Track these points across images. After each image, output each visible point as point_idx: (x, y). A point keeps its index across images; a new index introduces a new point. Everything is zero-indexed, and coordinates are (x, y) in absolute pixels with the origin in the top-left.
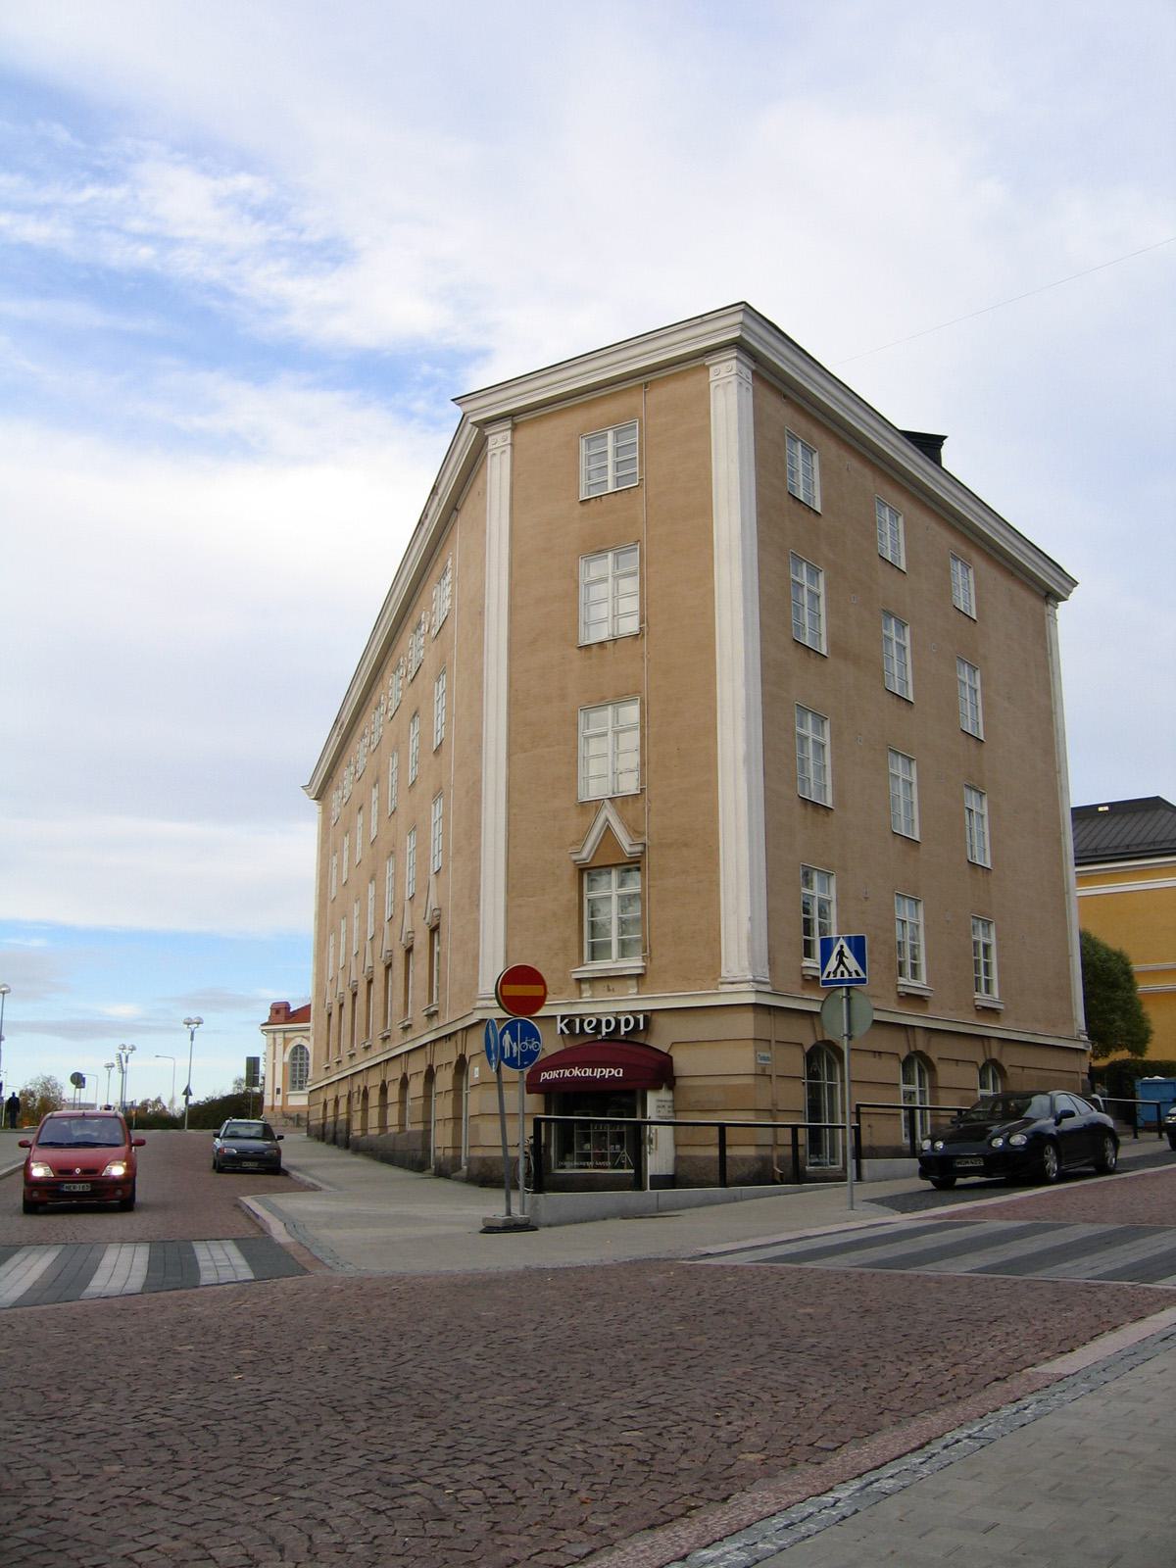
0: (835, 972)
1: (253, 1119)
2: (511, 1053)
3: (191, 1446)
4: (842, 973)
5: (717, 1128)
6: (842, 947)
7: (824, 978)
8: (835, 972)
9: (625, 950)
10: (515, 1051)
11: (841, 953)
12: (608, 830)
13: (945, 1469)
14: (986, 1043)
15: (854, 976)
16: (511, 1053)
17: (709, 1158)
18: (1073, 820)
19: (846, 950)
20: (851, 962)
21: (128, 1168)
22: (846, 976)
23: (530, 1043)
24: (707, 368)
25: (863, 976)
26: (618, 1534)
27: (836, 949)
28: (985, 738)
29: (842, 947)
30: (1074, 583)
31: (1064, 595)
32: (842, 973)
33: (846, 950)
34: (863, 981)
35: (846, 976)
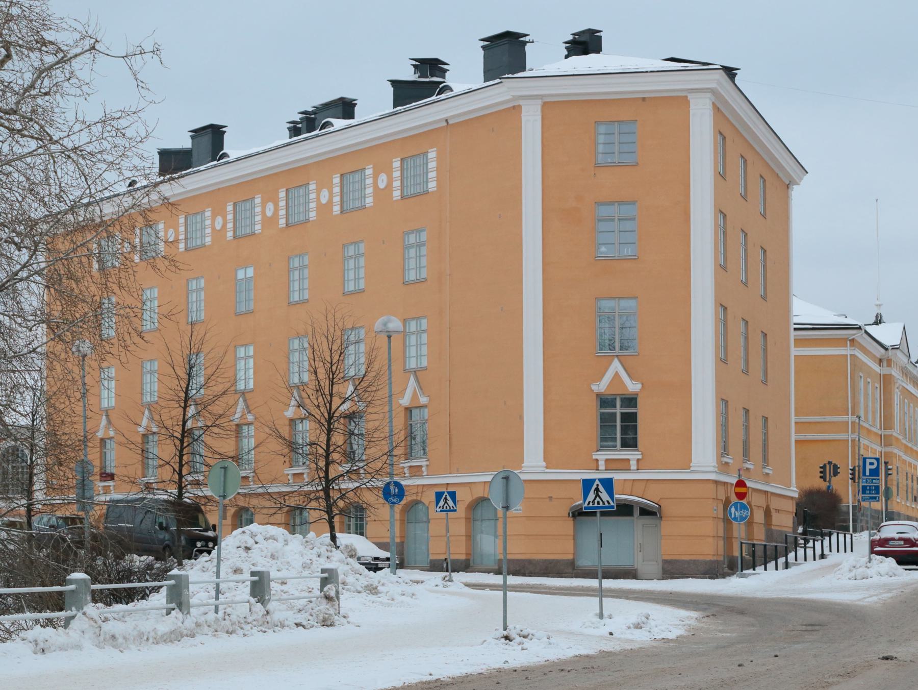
0: (593, 502)
1: (52, 585)
2: (735, 515)
4: (598, 502)
6: (598, 485)
7: (586, 505)
8: (593, 502)
10: (737, 514)
11: (597, 490)
12: (617, 375)
13: (393, 379)
14: (421, 410)
15: (452, 508)
16: (735, 515)
19: (448, 497)
20: (604, 496)
21: (260, 578)
22: (448, 508)
25: (455, 508)
27: (444, 496)
28: (848, 481)
29: (598, 485)
30: (807, 173)
31: (798, 181)
32: (598, 502)
33: (448, 497)
34: (455, 511)
35: (448, 508)
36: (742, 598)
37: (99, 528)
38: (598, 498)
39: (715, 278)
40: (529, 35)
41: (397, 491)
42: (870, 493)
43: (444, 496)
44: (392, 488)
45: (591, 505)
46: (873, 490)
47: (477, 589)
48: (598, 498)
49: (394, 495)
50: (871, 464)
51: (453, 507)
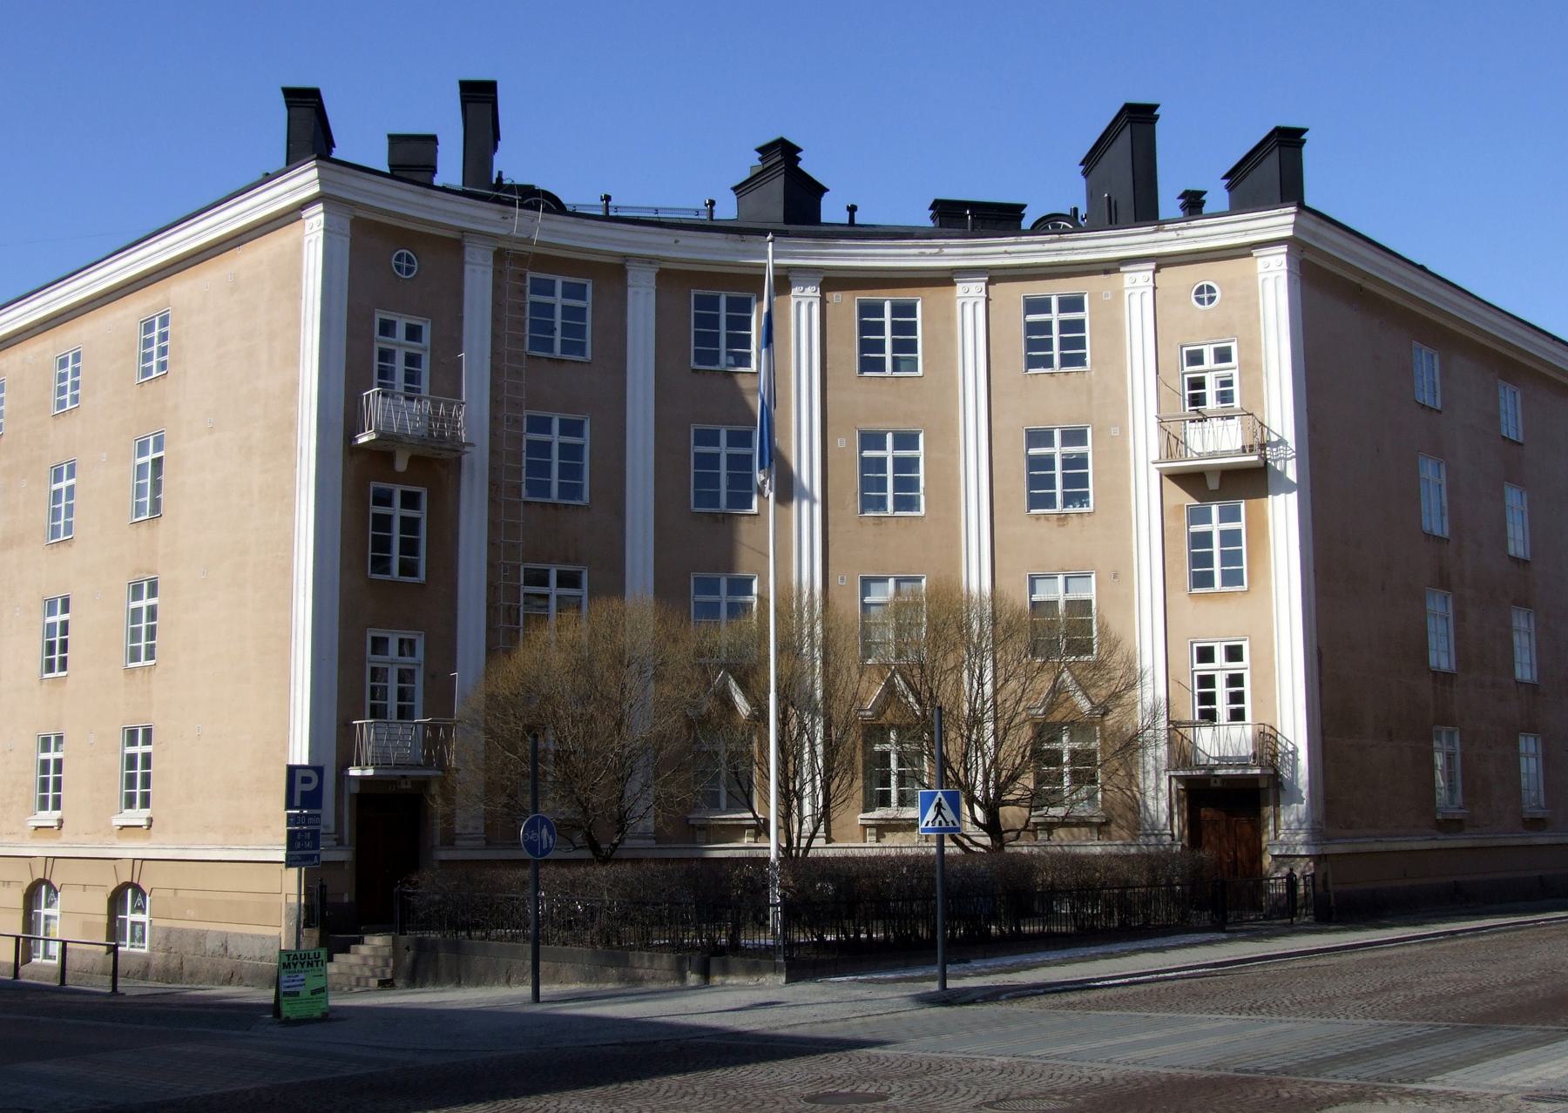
3: (910, 1089)
5: (14, 938)
9: (903, 801)
15: (951, 825)
16: (548, 845)
17: (554, 979)
18: (387, 336)
19: (944, 802)
23: (530, 834)
24: (954, 284)
25: (958, 825)
26: (1346, 1096)
29: (940, 799)
33: (944, 802)
36: (412, 1007)
37: (539, 638)
38: (940, 816)
39: (1307, 380)
42: (303, 848)
43: (936, 800)
45: (930, 825)
46: (307, 840)
47: (628, 1002)
48: (940, 816)
50: (306, 780)
51: (954, 824)
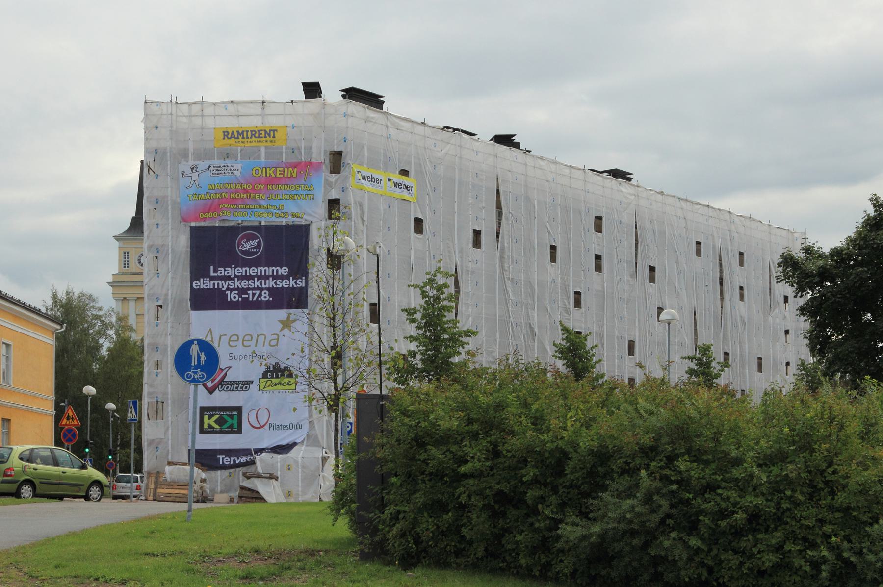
23: (195, 373)
40: (279, 321)
41: (203, 358)
44: (195, 349)
49: (198, 366)
